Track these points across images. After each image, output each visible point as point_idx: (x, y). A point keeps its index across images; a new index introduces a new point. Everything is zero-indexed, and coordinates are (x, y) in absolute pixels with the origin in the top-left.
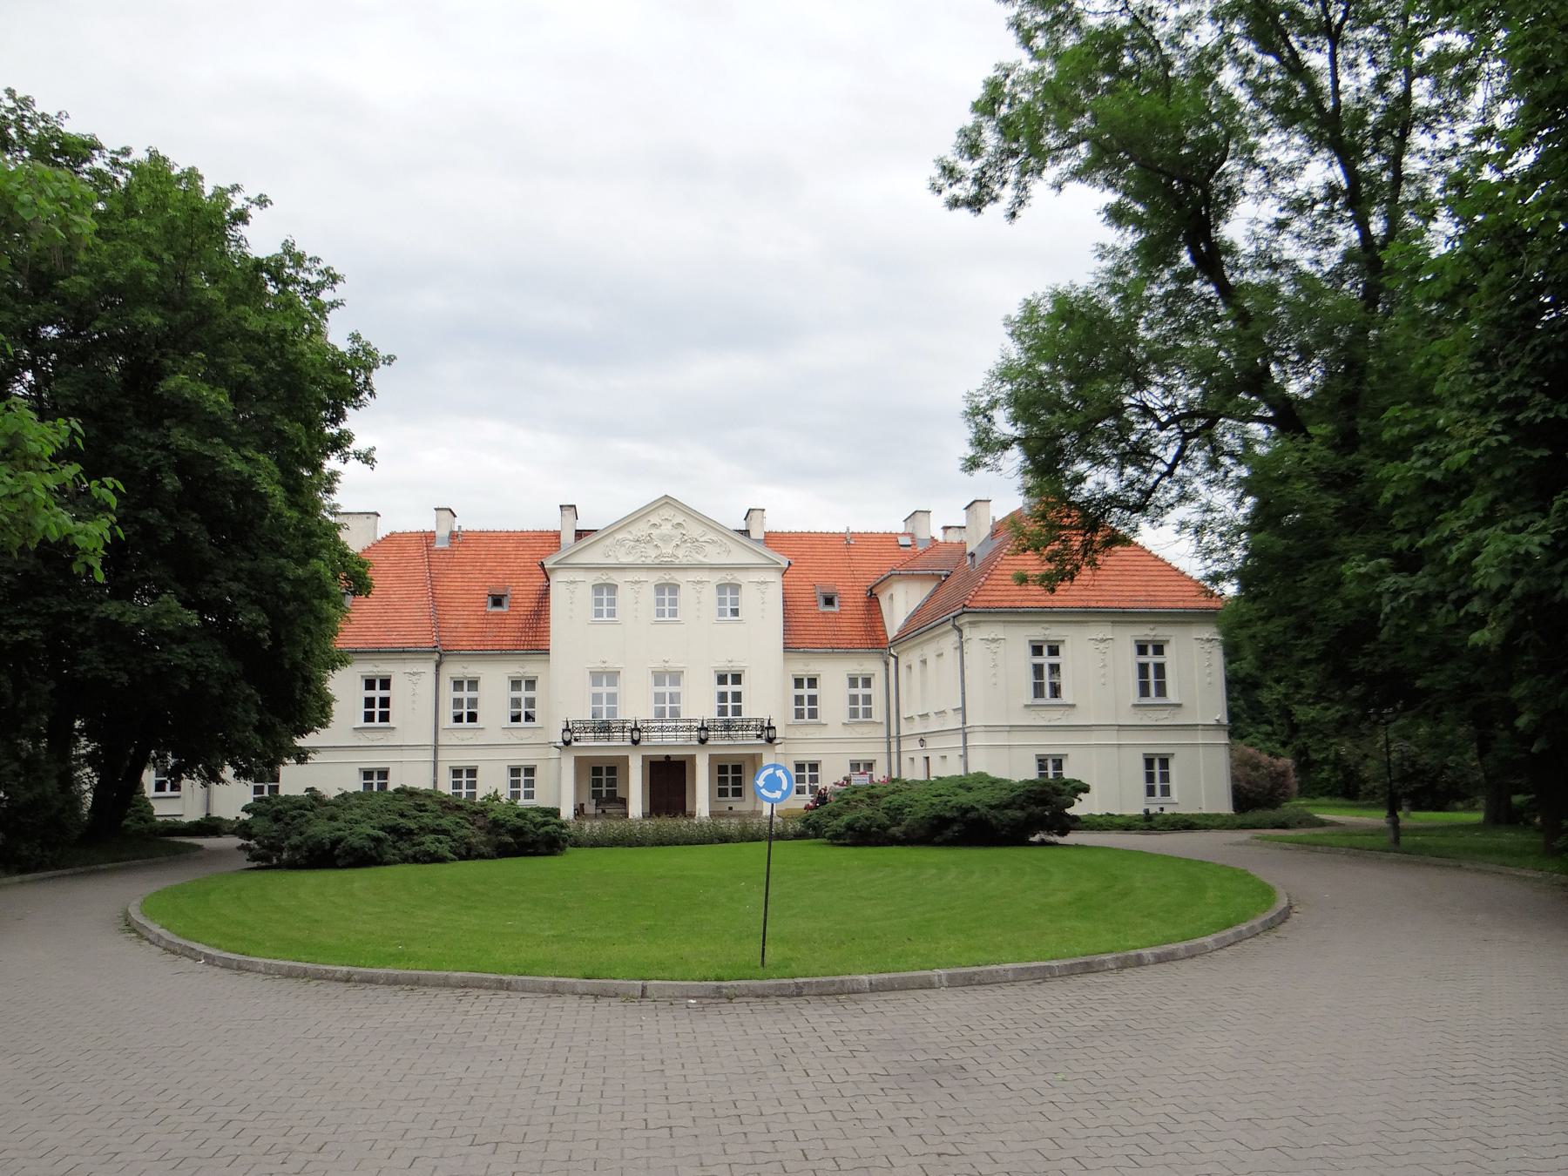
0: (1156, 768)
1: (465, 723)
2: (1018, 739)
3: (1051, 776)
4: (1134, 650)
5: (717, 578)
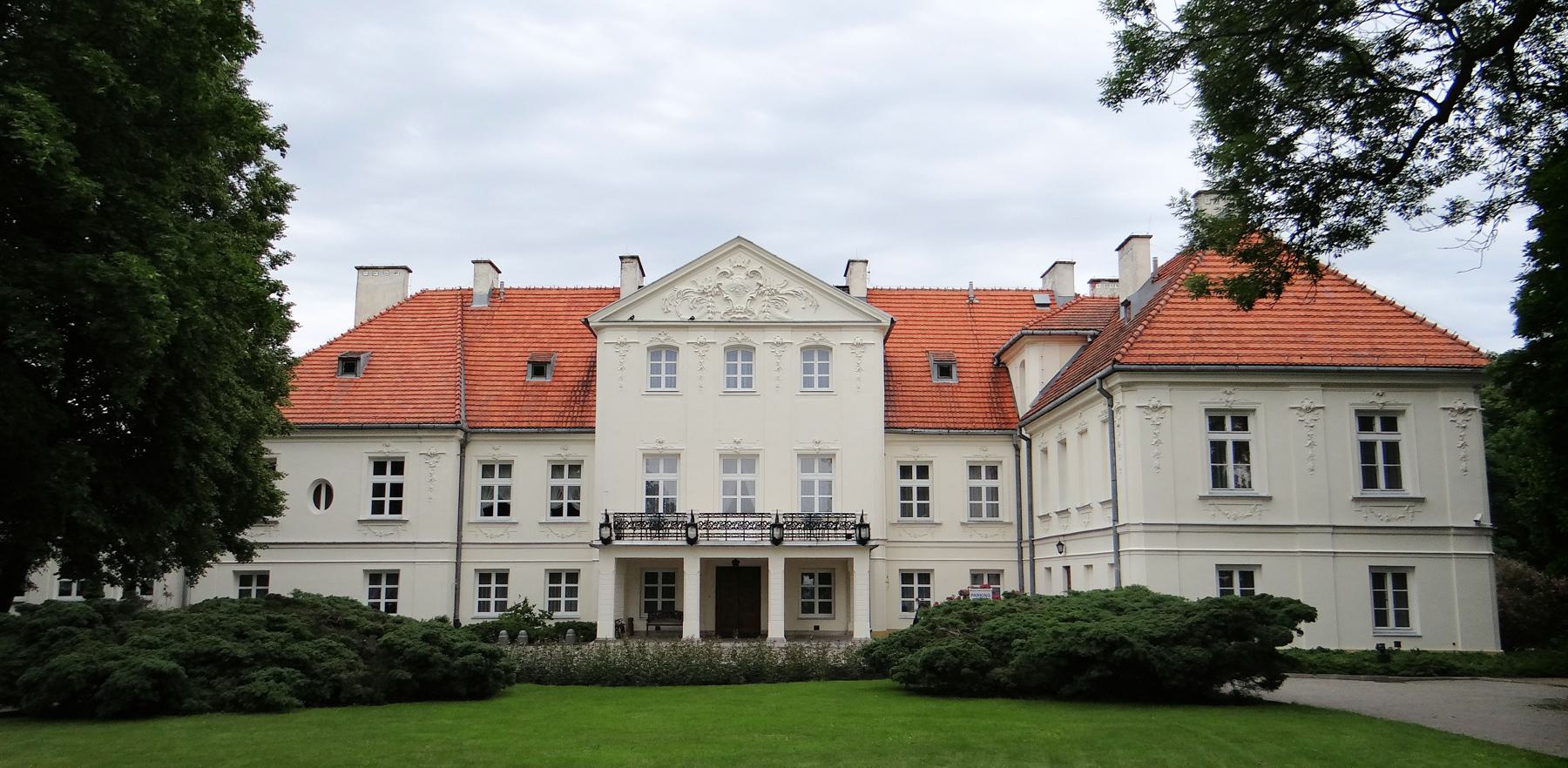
0: (1389, 588)
1: (495, 517)
2: (1191, 542)
3: (1237, 592)
4: (1354, 423)
5: (801, 339)
